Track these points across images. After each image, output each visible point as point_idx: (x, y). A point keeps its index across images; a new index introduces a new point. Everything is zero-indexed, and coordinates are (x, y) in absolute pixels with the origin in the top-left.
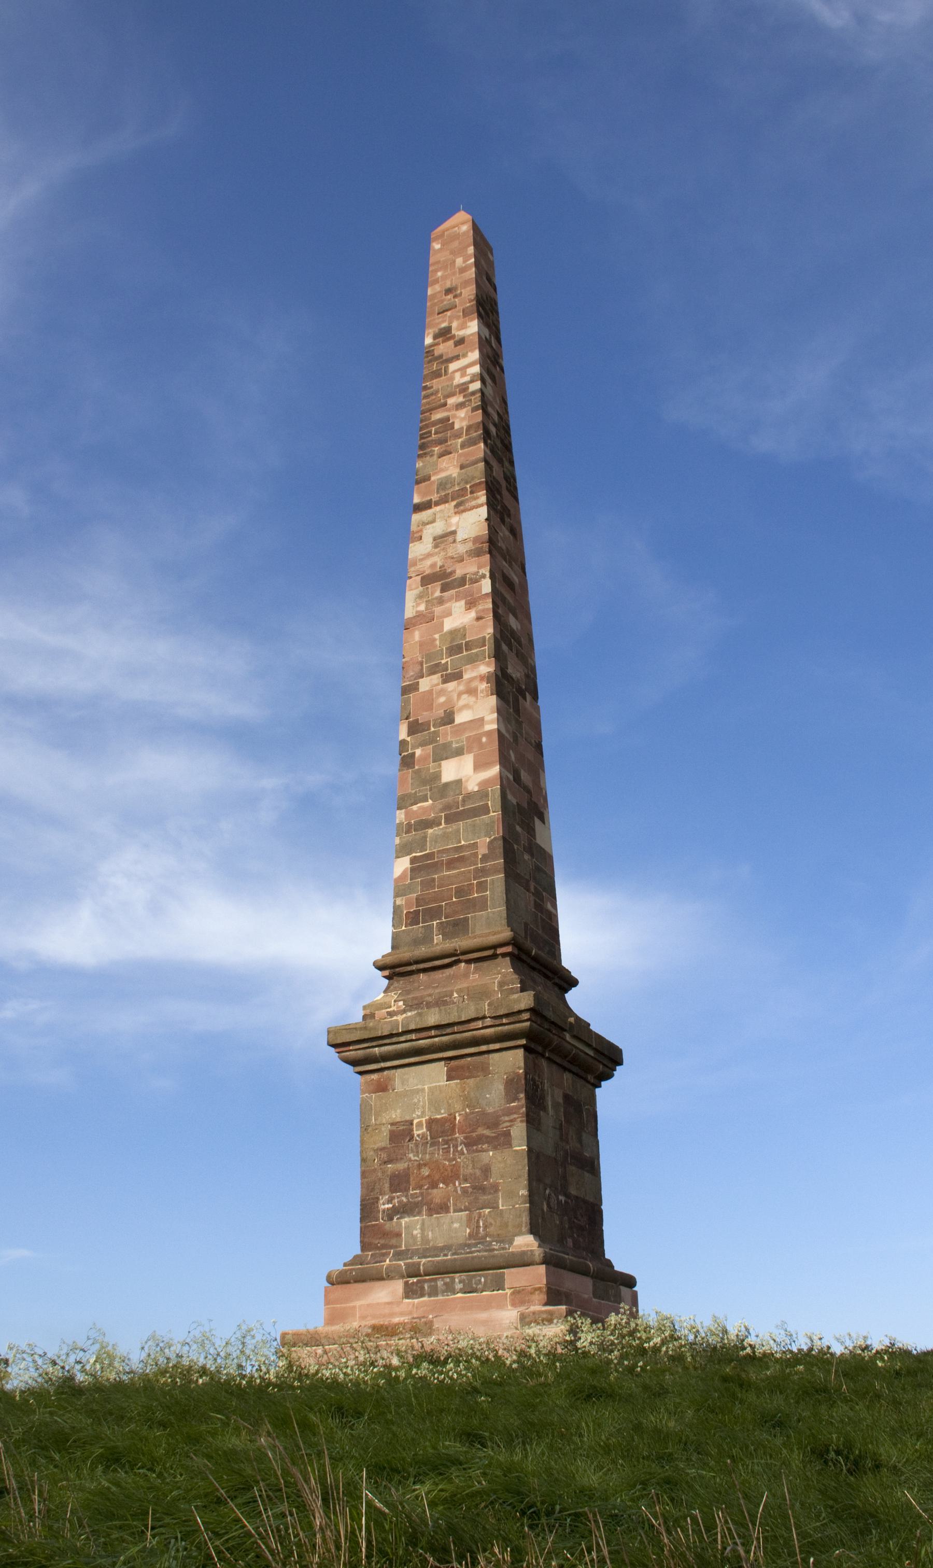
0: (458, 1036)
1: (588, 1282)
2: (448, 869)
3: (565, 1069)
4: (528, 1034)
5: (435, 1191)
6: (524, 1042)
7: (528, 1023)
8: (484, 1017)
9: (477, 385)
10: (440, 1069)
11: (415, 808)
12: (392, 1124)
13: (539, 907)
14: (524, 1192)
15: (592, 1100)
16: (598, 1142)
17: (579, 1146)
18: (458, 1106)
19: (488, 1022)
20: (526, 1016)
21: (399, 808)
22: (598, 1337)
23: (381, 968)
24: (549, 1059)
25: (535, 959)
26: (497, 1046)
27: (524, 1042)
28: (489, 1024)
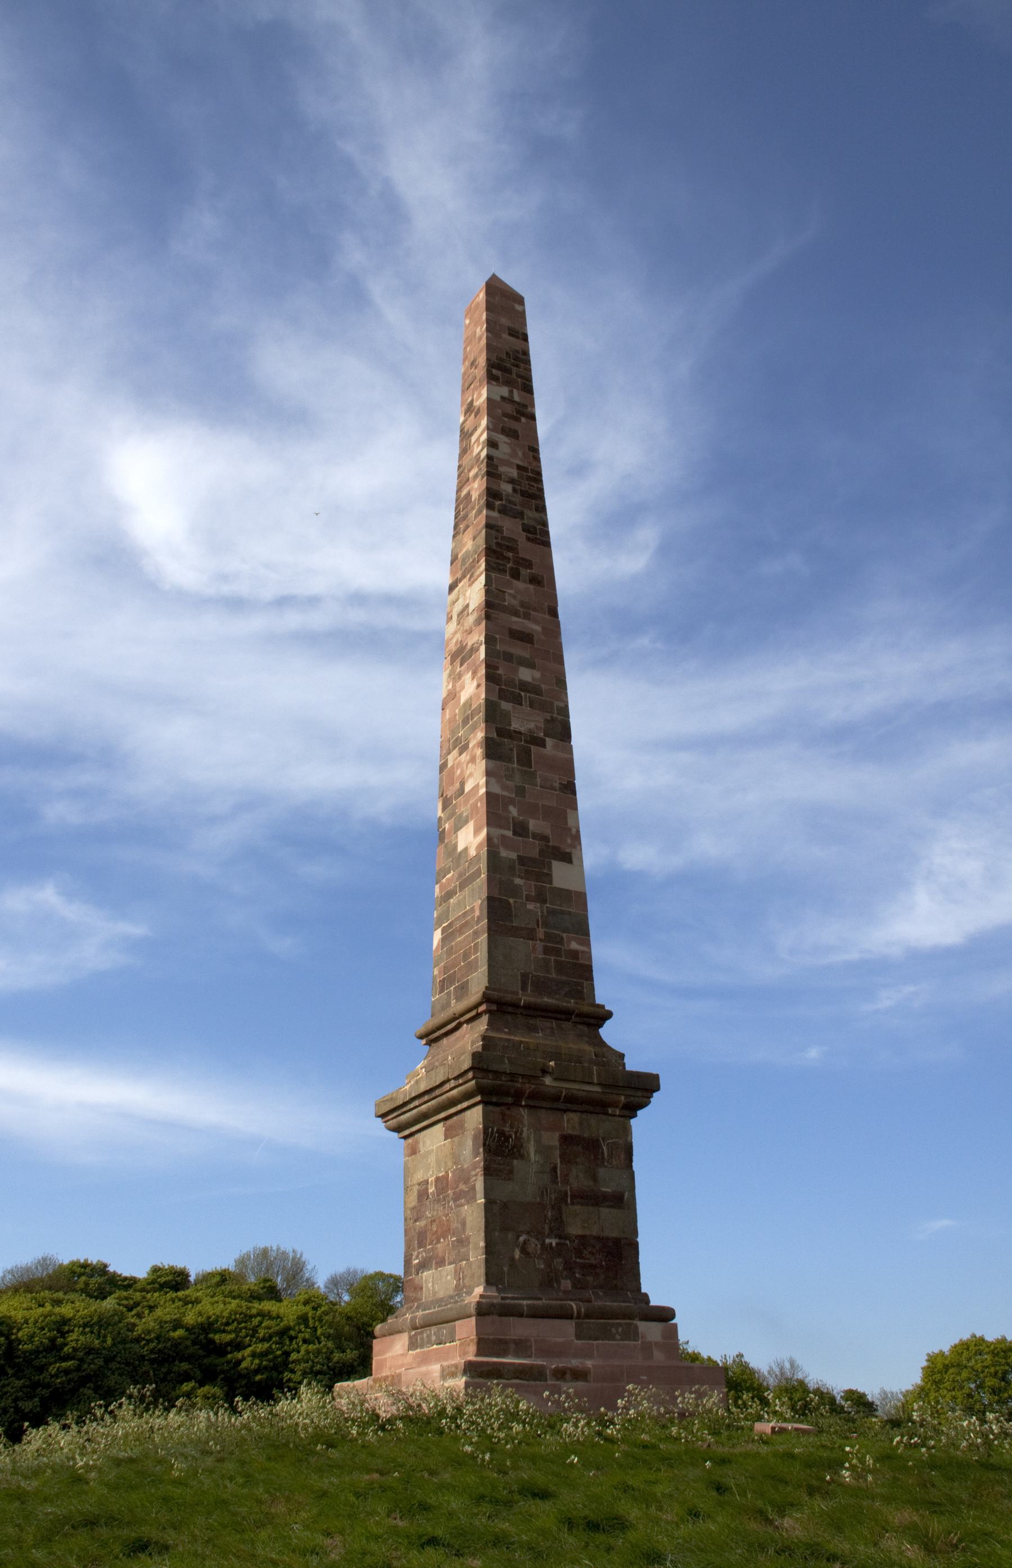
0: (439, 1099)
1: (569, 1327)
2: (461, 935)
3: (565, 1111)
4: (480, 1090)
5: (439, 1246)
6: (478, 1098)
7: (473, 1082)
8: (448, 1080)
9: (484, 453)
10: (439, 1129)
11: (444, 880)
12: (419, 1184)
13: (553, 946)
14: (482, 1244)
15: (627, 1131)
16: (633, 1173)
17: (591, 1183)
18: (450, 1164)
19: (453, 1083)
20: (470, 1075)
21: (518, 856)
22: (129, 1404)
23: (421, 1037)
24: (526, 1106)
25: (528, 1007)
26: (465, 1104)
27: (478, 1098)
28: (452, 1085)
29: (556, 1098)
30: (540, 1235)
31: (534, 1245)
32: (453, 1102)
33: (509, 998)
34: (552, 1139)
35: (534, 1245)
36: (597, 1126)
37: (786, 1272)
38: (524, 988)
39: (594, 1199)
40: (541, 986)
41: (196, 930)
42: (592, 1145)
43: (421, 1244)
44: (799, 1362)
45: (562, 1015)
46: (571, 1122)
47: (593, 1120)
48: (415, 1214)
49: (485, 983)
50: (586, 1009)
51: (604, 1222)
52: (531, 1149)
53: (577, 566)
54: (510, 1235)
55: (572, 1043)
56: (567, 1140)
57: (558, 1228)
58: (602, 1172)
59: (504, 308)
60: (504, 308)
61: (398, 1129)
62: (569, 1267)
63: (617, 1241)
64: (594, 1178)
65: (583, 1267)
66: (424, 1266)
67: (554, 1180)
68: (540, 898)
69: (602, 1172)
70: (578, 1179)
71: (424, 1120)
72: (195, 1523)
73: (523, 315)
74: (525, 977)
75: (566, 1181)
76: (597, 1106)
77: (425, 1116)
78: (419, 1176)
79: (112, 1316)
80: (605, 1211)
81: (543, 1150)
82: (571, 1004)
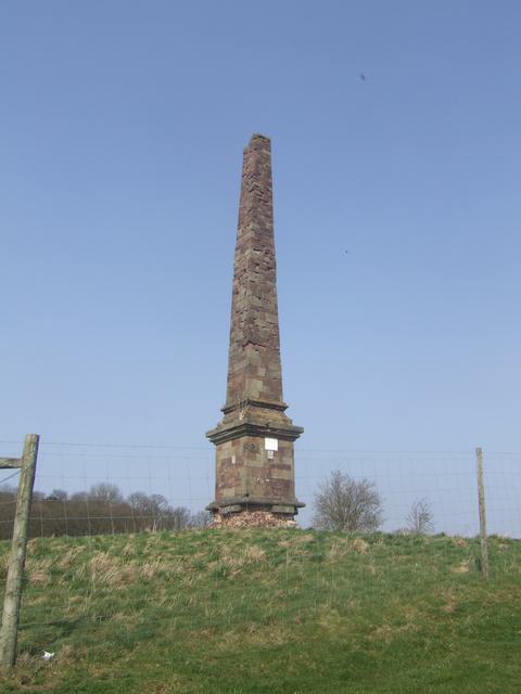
10: (230, 443)
31: (262, 482)
35: (262, 482)
40: (267, 397)
41: (8, 464)
45: (273, 407)
48: (219, 471)
51: (284, 475)
57: (270, 475)
58: (284, 459)
59: (261, 144)
60: (261, 144)
61: (214, 442)
62: (273, 488)
63: (288, 481)
64: (281, 460)
66: (223, 487)
69: (284, 459)
71: (225, 439)
72: (140, 565)
77: (225, 438)
79: (467, 628)
80: (285, 471)
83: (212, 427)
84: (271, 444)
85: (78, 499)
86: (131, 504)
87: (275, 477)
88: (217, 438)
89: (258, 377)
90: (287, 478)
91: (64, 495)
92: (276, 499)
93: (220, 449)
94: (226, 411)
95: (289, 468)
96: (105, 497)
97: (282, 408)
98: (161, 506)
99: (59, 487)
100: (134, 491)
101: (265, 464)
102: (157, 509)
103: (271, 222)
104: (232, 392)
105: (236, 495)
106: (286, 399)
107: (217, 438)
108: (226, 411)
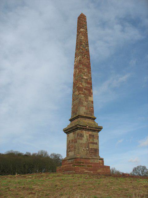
10: (72, 133)
29: (89, 129)
30: (86, 148)
32: (74, 129)
33: (82, 115)
34: (88, 135)
36: (94, 133)
37: (121, 154)
38: (84, 114)
39: (93, 143)
40: (87, 114)
42: (93, 136)
43: (69, 148)
44: (115, 168)
46: (90, 133)
47: (93, 132)
49: (10, 175)
50: (93, 117)
51: (94, 146)
52: (85, 136)
53: (97, 51)
54: (82, 148)
55: (90, 121)
56: (90, 135)
59: (82, 21)
60: (82, 21)
62: (89, 152)
63: (96, 149)
65: (91, 152)
67: (88, 140)
68: (87, 102)
70: (91, 140)
73: (86, 19)
74: (85, 112)
75: (89, 140)
76: (94, 131)
77: (70, 131)
78: (69, 139)
81: (87, 136)
82: (91, 116)
83: (65, 126)
84: (86, 134)
85: (34, 155)
86: (51, 157)
87: (90, 147)
88: (67, 131)
89: (83, 106)
90: (95, 148)
91: (30, 154)
92: (56, 158)
93: (68, 136)
94: (71, 120)
95: (96, 144)
96: (42, 155)
97: (94, 119)
98: (60, 158)
99: (45, 149)
100: (52, 153)
101: (86, 142)
102: (59, 159)
103: (88, 47)
104: (73, 112)
105: (74, 155)
106: (95, 115)
107: (67, 131)
108: (71, 120)
